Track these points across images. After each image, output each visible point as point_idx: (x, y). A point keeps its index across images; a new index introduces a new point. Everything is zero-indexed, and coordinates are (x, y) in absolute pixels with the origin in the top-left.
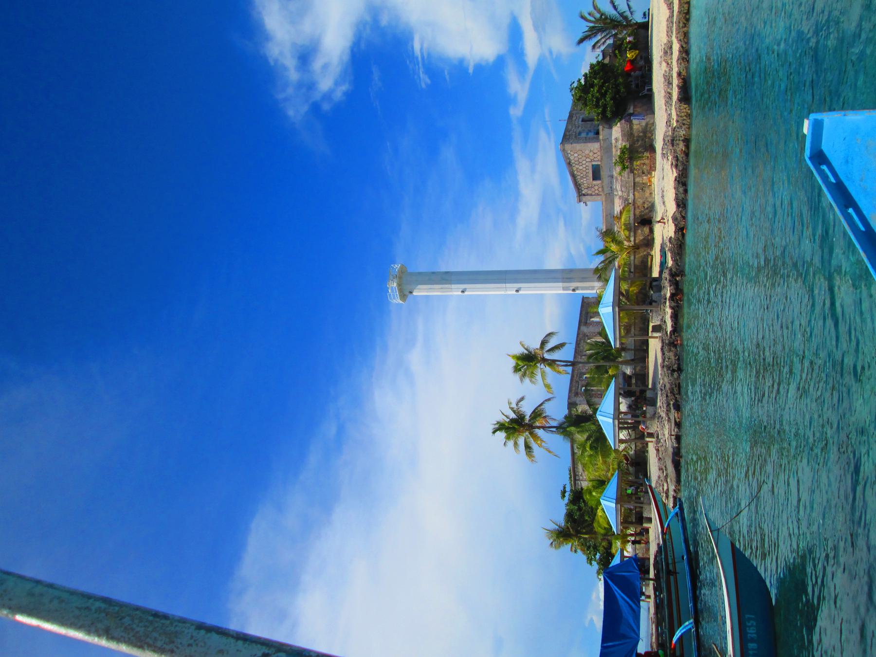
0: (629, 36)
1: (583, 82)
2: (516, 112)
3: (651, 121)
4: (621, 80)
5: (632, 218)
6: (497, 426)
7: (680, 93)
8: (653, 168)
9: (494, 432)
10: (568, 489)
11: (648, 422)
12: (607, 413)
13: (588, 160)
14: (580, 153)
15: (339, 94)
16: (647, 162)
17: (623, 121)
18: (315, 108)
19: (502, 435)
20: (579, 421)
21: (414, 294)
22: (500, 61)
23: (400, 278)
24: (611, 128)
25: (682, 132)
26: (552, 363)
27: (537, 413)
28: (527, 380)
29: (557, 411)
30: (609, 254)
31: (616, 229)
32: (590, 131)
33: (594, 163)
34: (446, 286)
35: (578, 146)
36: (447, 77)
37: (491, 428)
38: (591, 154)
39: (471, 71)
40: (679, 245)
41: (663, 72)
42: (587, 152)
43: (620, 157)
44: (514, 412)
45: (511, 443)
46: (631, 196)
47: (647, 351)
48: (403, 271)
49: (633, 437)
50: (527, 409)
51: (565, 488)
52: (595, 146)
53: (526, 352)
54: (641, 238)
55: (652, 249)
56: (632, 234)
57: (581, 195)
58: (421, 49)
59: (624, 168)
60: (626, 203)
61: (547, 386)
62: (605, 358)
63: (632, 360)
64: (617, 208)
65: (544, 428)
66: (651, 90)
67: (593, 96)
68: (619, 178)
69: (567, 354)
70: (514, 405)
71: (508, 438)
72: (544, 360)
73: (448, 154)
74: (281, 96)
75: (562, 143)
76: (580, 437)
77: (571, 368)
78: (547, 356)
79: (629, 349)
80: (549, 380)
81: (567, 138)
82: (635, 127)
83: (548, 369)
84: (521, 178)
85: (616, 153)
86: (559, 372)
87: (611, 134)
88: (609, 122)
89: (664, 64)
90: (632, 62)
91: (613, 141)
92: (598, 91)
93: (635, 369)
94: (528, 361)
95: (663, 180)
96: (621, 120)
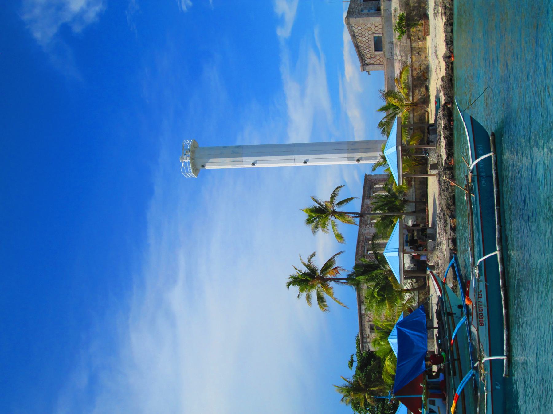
2: (283, 33)
5: (410, 78)
6: (291, 280)
8: (427, 33)
9: (288, 286)
10: (355, 356)
11: (429, 254)
12: (395, 256)
13: (370, 33)
14: (363, 26)
15: (92, 15)
18: (65, 30)
19: (295, 289)
20: (369, 269)
21: (207, 167)
23: (193, 152)
26: (341, 214)
27: (328, 266)
28: (320, 231)
29: (346, 264)
30: (391, 111)
31: (396, 90)
33: (375, 35)
34: (238, 158)
35: (360, 20)
37: (285, 285)
38: (373, 27)
40: (449, 82)
42: (369, 25)
43: (399, 24)
44: (307, 266)
45: (304, 295)
46: (409, 59)
47: (426, 203)
48: (195, 146)
49: (416, 286)
50: (319, 263)
51: (352, 357)
52: (377, 20)
53: (317, 205)
54: (419, 97)
55: (428, 106)
56: (411, 94)
57: (364, 64)
59: (402, 33)
60: (405, 66)
61: (339, 236)
62: (391, 210)
63: (414, 212)
64: (397, 72)
65: (334, 280)
68: (398, 44)
69: (356, 206)
70: (307, 263)
71: (302, 290)
72: (334, 213)
73: (212, 75)
74: (26, 17)
78: (337, 209)
79: (410, 201)
80: (339, 231)
81: (350, 14)
83: (338, 221)
84: (290, 103)
85: (395, 21)
86: (349, 222)
91: (393, 11)
94: (319, 214)
95: (436, 42)
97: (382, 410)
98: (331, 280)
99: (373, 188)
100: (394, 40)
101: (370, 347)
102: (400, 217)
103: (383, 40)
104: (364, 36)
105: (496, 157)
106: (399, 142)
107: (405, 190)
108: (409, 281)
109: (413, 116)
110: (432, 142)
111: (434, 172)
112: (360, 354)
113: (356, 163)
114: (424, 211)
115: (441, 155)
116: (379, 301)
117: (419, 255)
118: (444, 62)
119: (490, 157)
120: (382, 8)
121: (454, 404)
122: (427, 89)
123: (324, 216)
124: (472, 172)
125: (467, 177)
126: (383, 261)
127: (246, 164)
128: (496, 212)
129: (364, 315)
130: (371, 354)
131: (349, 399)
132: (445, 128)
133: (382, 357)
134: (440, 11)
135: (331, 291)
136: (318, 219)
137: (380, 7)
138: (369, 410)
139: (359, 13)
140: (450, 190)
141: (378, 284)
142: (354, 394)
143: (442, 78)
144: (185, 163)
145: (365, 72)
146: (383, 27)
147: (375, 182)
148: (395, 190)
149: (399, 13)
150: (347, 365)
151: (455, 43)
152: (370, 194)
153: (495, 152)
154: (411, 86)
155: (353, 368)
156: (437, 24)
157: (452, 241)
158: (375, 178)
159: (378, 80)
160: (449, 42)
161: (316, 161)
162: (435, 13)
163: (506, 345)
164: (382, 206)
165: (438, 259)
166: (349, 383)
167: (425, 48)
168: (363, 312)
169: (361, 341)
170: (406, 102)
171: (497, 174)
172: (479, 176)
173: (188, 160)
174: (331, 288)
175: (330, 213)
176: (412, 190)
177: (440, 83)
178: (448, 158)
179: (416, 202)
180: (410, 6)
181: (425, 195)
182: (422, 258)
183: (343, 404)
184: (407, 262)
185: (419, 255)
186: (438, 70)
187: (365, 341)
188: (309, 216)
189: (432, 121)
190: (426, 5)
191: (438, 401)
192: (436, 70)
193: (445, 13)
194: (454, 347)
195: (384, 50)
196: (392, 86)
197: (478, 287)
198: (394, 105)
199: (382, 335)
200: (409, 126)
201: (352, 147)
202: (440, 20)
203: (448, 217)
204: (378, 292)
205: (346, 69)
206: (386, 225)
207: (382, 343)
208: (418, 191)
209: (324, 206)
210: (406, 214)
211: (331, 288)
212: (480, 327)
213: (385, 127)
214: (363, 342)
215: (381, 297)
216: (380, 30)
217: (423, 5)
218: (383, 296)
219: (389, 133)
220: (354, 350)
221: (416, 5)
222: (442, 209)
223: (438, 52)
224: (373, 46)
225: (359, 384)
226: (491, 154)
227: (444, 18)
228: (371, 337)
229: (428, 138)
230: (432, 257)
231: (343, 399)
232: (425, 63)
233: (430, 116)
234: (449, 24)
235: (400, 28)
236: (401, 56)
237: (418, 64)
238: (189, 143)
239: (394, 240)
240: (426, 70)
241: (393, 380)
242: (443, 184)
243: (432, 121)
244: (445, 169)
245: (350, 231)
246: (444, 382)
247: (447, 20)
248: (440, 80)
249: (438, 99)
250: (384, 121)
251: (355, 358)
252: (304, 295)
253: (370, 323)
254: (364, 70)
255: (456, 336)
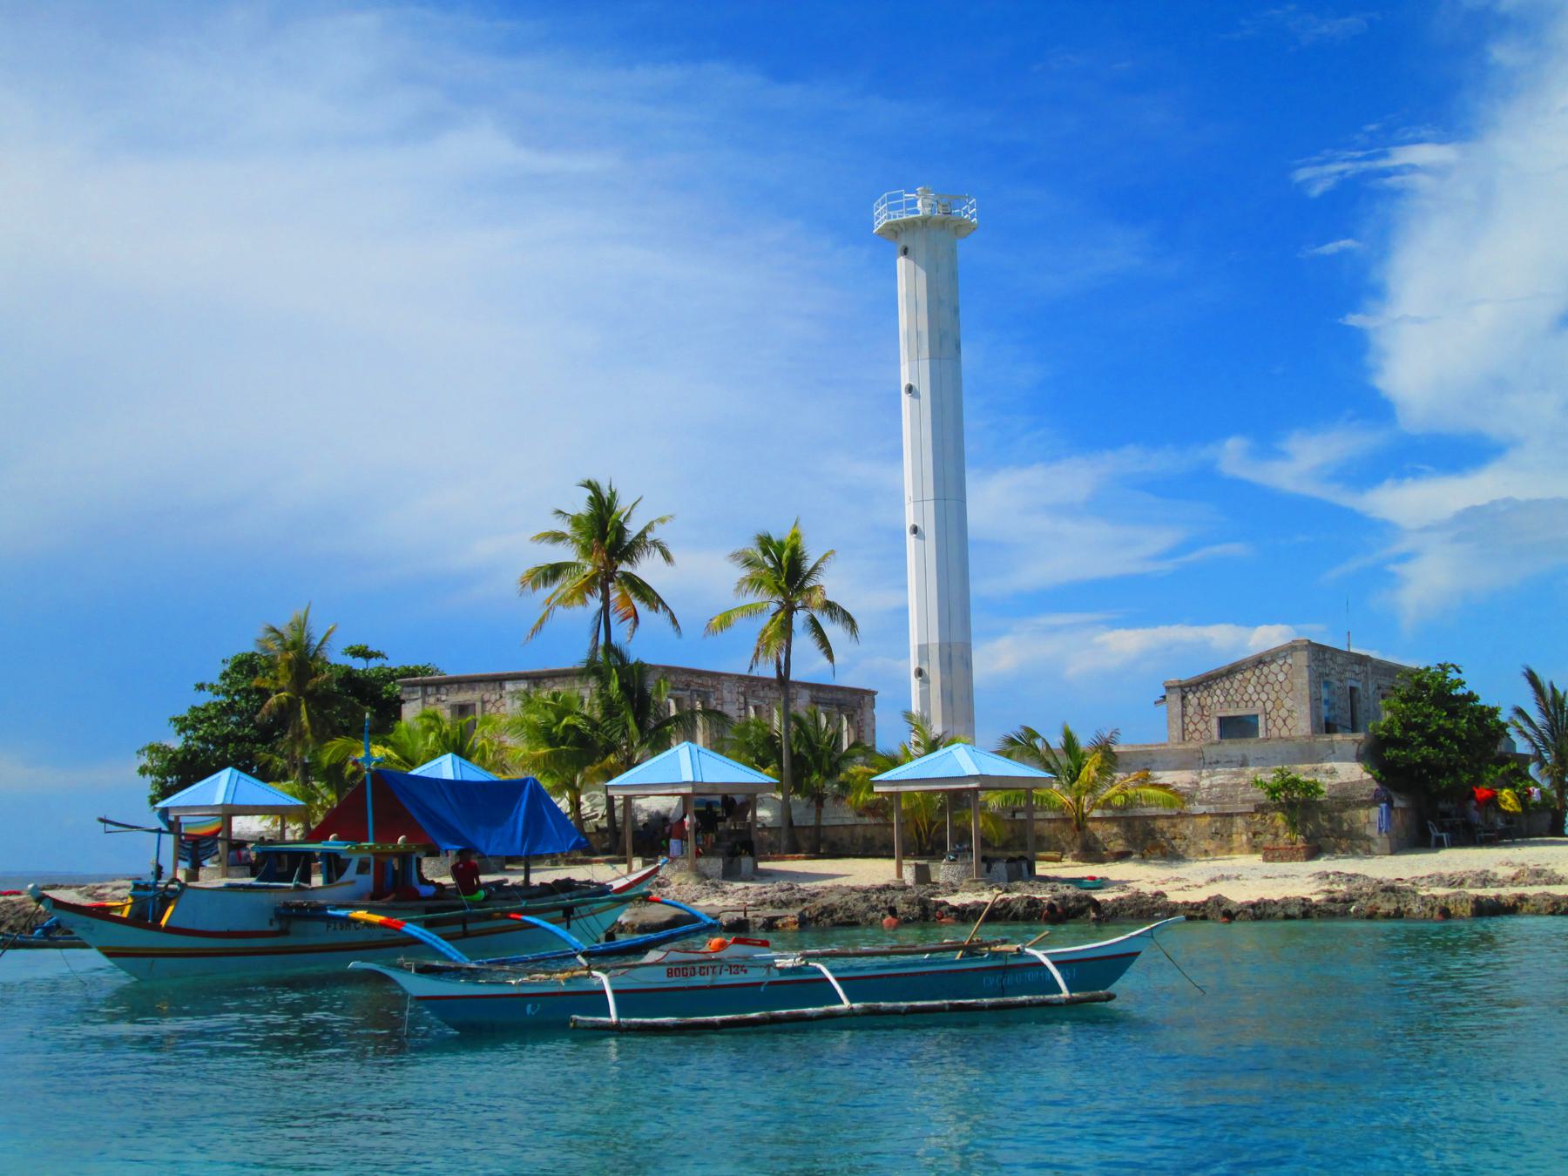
0: (1541, 792)
1: (1460, 691)
2: (1232, 456)
3: (1374, 848)
4: (1466, 778)
5: (1153, 811)
6: (606, 494)
7: (1489, 900)
8: (1271, 855)
9: (589, 485)
10: (374, 663)
12: (682, 767)
13: (1269, 705)
16: (1281, 842)
17: (1375, 786)
19: (580, 504)
20: (637, 705)
21: (901, 262)
22: (1377, 409)
24: (1359, 758)
25: (1415, 907)
29: (647, 642)
30: (1064, 760)
31: (1119, 775)
32: (1332, 707)
33: (1261, 720)
34: (926, 347)
35: (1302, 680)
36: (1330, 248)
38: (1283, 713)
39: (1354, 320)
40: (1146, 909)
41: (1493, 870)
42: (1288, 703)
43: (1295, 782)
44: (642, 535)
45: (566, 528)
46: (1203, 809)
47: (815, 854)
50: (647, 568)
51: (378, 655)
54: (1099, 835)
55: (1076, 858)
56: (1109, 813)
57: (1185, 689)
58: (1413, 168)
59: (1273, 791)
61: (726, 621)
62: (797, 760)
63: (791, 823)
64: (1166, 777)
66: (1439, 845)
67: (1428, 716)
68: (1242, 780)
69: (808, 665)
70: (650, 536)
71: (576, 521)
72: (789, 609)
73: (1119, 252)
75: (1310, 644)
76: (586, 696)
77: (772, 674)
78: (799, 618)
79: (819, 813)
80: (739, 623)
81: (1319, 653)
82: (1362, 813)
84: (1035, 475)
85: (1302, 772)
87: (1344, 759)
88: (1374, 753)
89: (1511, 872)
90: (1493, 801)
91: (1328, 766)
92: (1441, 728)
93: (764, 827)
94: (786, 571)
95: (1250, 877)
96: (1379, 781)
97: (236, 736)
98: (606, 599)
99: (840, 713)
100: (1250, 770)
101: (413, 704)
102: (778, 787)
103: (1252, 740)
104: (1259, 688)
105: (1060, 1004)
106: (990, 783)
107: (852, 798)
108: (601, 810)
109: (1050, 820)
110: (988, 870)
111: (909, 876)
112: (390, 677)
113: (914, 665)
114: (794, 850)
115: (955, 891)
116: (550, 729)
117: (682, 836)
118: (1205, 898)
119: (1059, 991)
120: (1338, 737)
121: (376, 918)
122: (1122, 857)
123: (782, 583)
124: (1020, 953)
125: (1004, 942)
126: (659, 743)
127: (912, 368)
128: (936, 1003)
129: (502, 688)
130: (390, 710)
131: (274, 646)
132: (1033, 903)
133: (391, 737)
134: (1335, 887)
135: (576, 600)
136: (771, 566)
137: (1335, 731)
138: (234, 701)
139: (1321, 675)
140: (871, 915)
141: (596, 726)
142: (289, 662)
143: (1160, 894)
144: (914, 203)
145: (1164, 693)
146: (1287, 739)
147: (857, 718)
148: (852, 770)
149: (1325, 782)
150: (356, 642)
151: (1260, 924)
152: (825, 704)
153: (1070, 1002)
154: (1130, 813)
155: (349, 657)
156: (1300, 881)
157: (739, 920)
158: (867, 716)
159: (1146, 727)
160: (1259, 911)
161: (919, 559)
162: (1327, 876)
163: (642, 1024)
164: (808, 738)
165: (674, 886)
166: (319, 648)
167: (1230, 850)
168: (509, 686)
169: (425, 681)
170: (1085, 800)
171: (1022, 1005)
172: (1005, 969)
173: (922, 208)
174: (584, 602)
175: (787, 599)
176: (849, 817)
177: (1148, 889)
178: (954, 909)
179: (818, 828)
180: (1341, 811)
181: (837, 851)
182: (674, 844)
183: (260, 632)
184: (650, 805)
185: (682, 836)
186: (1179, 885)
187: (430, 690)
188: (781, 544)
189: (1041, 869)
190: (1343, 852)
191: (367, 881)
192: (1178, 879)
193: (1333, 900)
194: (504, 922)
195: (1226, 742)
196: (1128, 764)
197: (756, 964)
198: (1079, 768)
199: (451, 737)
200: (1030, 809)
201: (955, 656)
202: (1313, 887)
203: (800, 910)
204: (575, 727)
205: (1131, 633)
206: (762, 752)
207: (432, 736)
208: (845, 834)
209: (809, 584)
210: (786, 799)
211: (584, 602)
212: (664, 969)
213: (1021, 745)
214: (425, 685)
215: (560, 734)
216: (1275, 732)
217: (1344, 844)
218: (563, 741)
219: (1009, 756)
220: (395, 662)
221: (1345, 827)
222: (815, 895)
223: (1224, 883)
224: (1232, 714)
225: (316, 675)
226: (1065, 993)
227: (1321, 897)
228: (441, 706)
229: (998, 859)
230: (680, 870)
231: (274, 630)
232: (1191, 851)
233: (1051, 864)
234: (1307, 910)
235: (1285, 785)
236: (1211, 787)
237: (1187, 832)
238: (969, 212)
239: (727, 772)
240: (1171, 855)
241: (330, 767)
242: (883, 897)
243: (1041, 869)
244: (923, 903)
245: (736, 656)
246: (416, 896)
247: (1316, 906)
248: (1154, 889)
249: (1102, 884)
250: (1039, 743)
251: (374, 663)
252: (566, 528)
253: (479, 705)
254: (1168, 688)
255: (536, 926)
